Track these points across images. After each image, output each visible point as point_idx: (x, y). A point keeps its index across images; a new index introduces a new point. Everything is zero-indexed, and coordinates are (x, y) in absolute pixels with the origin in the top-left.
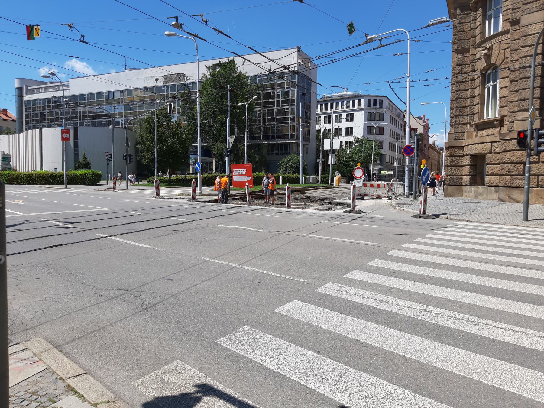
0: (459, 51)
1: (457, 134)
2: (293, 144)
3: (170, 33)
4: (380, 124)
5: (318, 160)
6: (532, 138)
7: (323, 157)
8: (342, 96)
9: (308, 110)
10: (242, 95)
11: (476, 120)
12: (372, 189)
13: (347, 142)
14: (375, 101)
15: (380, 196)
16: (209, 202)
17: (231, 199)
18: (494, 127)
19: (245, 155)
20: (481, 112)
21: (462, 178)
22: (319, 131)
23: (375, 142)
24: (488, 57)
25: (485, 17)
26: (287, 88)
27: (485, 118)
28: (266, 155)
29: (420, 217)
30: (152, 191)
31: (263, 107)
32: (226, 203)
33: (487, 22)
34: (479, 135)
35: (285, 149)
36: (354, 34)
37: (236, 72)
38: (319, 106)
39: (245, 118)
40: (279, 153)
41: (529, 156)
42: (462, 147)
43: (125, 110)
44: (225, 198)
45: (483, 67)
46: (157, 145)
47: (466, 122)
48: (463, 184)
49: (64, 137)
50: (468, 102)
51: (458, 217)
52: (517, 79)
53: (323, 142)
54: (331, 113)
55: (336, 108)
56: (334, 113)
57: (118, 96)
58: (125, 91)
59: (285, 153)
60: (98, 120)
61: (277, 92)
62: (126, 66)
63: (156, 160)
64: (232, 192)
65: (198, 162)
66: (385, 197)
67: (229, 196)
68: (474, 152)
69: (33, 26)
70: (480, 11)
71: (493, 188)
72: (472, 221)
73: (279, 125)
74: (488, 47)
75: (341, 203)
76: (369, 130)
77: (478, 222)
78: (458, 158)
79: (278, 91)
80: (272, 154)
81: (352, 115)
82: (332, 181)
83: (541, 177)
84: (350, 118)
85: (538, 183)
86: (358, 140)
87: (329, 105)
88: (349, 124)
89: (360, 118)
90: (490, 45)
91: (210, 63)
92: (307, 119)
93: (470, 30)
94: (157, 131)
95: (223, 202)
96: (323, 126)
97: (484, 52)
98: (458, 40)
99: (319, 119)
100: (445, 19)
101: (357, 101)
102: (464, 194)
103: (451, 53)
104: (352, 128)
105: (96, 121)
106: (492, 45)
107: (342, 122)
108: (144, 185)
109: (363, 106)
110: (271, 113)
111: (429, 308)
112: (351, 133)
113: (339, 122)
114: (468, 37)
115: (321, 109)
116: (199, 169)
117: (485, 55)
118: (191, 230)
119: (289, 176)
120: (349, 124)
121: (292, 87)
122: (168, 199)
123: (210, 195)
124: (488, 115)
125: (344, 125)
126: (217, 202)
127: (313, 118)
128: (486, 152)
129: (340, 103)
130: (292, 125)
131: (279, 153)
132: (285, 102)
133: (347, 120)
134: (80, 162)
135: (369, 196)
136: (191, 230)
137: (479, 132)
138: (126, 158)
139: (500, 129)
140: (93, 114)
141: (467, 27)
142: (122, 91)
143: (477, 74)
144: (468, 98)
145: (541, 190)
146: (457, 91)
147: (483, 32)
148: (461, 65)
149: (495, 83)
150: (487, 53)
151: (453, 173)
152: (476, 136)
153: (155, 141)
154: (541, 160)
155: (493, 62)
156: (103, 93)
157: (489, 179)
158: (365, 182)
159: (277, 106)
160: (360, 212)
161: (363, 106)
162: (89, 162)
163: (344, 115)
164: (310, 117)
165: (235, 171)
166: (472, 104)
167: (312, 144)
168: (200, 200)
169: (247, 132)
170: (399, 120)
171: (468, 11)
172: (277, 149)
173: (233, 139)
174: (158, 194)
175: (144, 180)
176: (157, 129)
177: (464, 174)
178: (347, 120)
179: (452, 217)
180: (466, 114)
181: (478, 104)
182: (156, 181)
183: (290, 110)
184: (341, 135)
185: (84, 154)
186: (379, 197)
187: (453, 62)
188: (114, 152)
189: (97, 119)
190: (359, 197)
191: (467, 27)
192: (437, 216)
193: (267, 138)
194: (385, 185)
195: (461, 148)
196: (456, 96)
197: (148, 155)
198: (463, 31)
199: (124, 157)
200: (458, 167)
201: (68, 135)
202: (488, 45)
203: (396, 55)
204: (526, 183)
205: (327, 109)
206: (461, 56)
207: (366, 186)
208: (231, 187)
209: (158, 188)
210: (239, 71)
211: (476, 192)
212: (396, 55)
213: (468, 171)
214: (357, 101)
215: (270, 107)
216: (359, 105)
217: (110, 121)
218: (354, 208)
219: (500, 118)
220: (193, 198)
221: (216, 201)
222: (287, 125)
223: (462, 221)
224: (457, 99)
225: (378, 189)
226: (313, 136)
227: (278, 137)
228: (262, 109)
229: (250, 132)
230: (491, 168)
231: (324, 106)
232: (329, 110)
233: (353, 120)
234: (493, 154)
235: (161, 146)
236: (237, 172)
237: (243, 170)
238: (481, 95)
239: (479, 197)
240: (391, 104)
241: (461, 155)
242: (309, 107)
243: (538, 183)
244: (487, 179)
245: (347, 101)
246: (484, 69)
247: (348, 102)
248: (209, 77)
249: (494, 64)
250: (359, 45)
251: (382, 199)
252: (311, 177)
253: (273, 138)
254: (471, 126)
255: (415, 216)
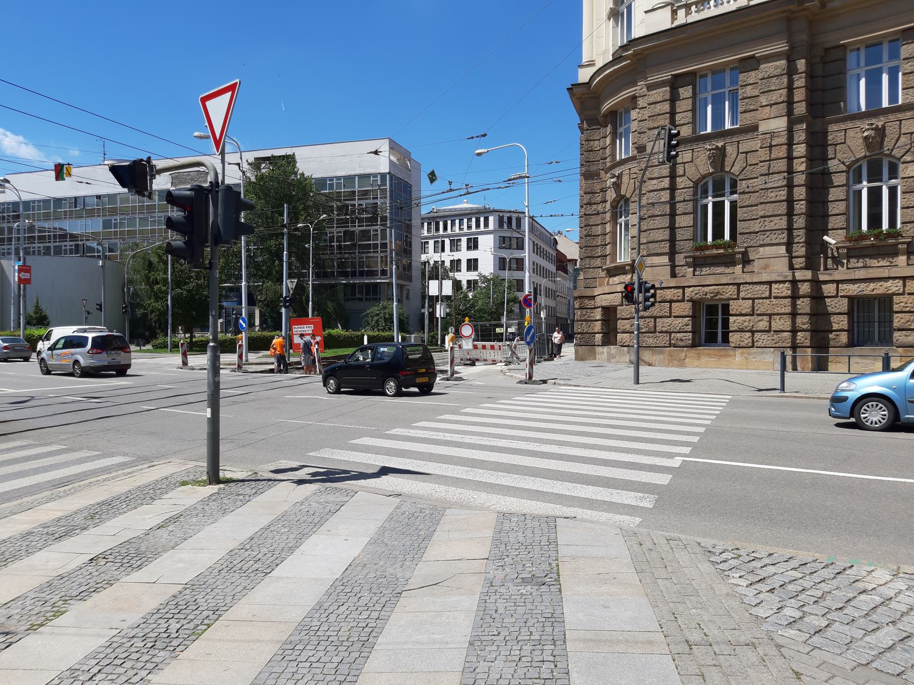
0: (588, 175)
1: (588, 280)
2: (386, 284)
3: (202, 134)
4: (517, 254)
5: (423, 311)
6: (640, 291)
7: (430, 306)
8: (461, 209)
9: (408, 232)
10: (305, 209)
11: (609, 264)
12: (484, 351)
13: (469, 282)
14: (510, 219)
15: (495, 361)
16: (261, 372)
17: (293, 368)
18: (625, 273)
19: (310, 303)
20: (614, 254)
21: (594, 336)
22: (424, 263)
23: (510, 282)
24: (617, 186)
25: (615, 135)
26: (373, 198)
27: (618, 261)
28: (342, 302)
29: (526, 383)
30: (177, 359)
31: (337, 227)
32: (287, 373)
33: (618, 141)
34: (611, 283)
35: (374, 292)
36: (435, 183)
37: (296, 173)
38: (426, 224)
39: (310, 246)
40: (364, 299)
41: (637, 311)
42: (593, 297)
43: (104, 228)
44: (284, 365)
45: (613, 197)
46: (172, 289)
47: (597, 266)
48: (596, 344)
49: (23, 278)
50: (599, 241)
51: (567, 382)
52: (646, 216)
53: (428, 282)
54: (443, 236)
55: (452, 229)
56: (448, 236)
57: (93, 204)
58: (105, 196)
59: (374, 299)
60: (55, 244)
61: (360, 205)
62: (105, 154)
63: (170, 313)
64: (292, 360)
65: (243, 316)
66: (501, 362)
67: (290, 364)
68: (604, 304)
69: (63, 165)
70: (609, 129)
71: (626, 349)
72: (579, 386)
73: (363, 255)
74: (617, 175)
75: (443, 371)
76: (502, 264)
77: (585, 386)
78: (589, 310)
79: (361, 202)
80: (352, 299)
81: (476, 241)
82: (443, 341)
83: (673, 335)
84: (473, 244)
85: (670, 342)
86: (485, 279)
87: (441, 224)
88: (472, 254)
89: (487, 242)
90: (619, 172)
91: (250, 157)
92: (406, 250)
93: (599, 150)
94: (173, 268)
95: (280, 371)
96: (431, 256)
97: (613, 180)
98: (586, 162)
99: (426, 246)
100: (524, 175)
101: (482, 219)
102: (598, 356)
103: (578, 176)
104: (476, 260)
105: (52, 245)
106: (622, 172)
107: (461, 251)
108: (148, 351)
109: (491, 226)
110: (349, 235)
111: (463, 436)
112: (476, 268)
113: (457, 250)
114: (597, 159)
115: (429, 230)
116: (244, 326)
117: (614, 183)
118: (253, 401)
119: (378, 335)
120: (472, 254)
121: (381, 198)
122: (201, 369)
123: (261, 364)
124: (620, 259)
125: (464, 255)
126: (274, 373)
127: (416, 246)
128: (617, 304)
129: (457, 221)
130: (382, 254)
131: (364, 299)
132: (373, 220)
133: (469, 248)
134: (30, 315)
135: (482, 361)
136: (253, 401)
137: (611, 279)
138: (126, 311)
139: (632, 276)
140: (47, 234)
141: (596, 145)
142: (99, 197)
143: (608, 205)
144: (599, 236)
145: (673, 350)
146: (585, 226)
147: (613, 155)
148: (589, 193)
149: (627, 219)
150: (616, 182)
151: (584, 330)
152: (608, 284)
153: (168, 283)
154: (673, 314)
155: (623, 193)
156: (65, 199)
157: (621, 337)
158: (476, 343)
159: (359, 226)
160: (461, 379)
161: (491, 226)
162: (45, 315)
163: (464, 240)
164: (411, 243)
165: (297, 329)
166: (603, 243)
167: (416, 284)
168: (249, 370)
169: (313, 268)
170: (547, 248)
171: (597, 125)
172: (361, 292)
173: (295, 284)
174: (185, 363)
175: (148, 342)
176: (173, 265)
177: (596, 331)
178: (469, 248)
179: (560, 382)
180: (596, 255)
181: (609, 243)
182: (182, 344)
183: (379, 232)
184: (460, 271)
185: (37, 302)
186: (494, 362)
187: (581, 189)
188: (104, 302)
189: (54, 242)
190: (469, 362)
191: (596, 145)
192: (545, 382)
193: (345, 275)
194: (500, 346)
195: (591, 298)
196: (585, 233)
197: (158, 305)
198: (592, 151)
199: (123, 308)
200: (589, 323)
201: (28, 274)
202: (617, 172)
203: (500, 188)
204: (635, 341)
205: (437, 230)
206: (590, 182)
207: (477, 348)
208: (291, 351)
209: (185, 355)
210: (300, 172)
211: (609, 354)
212: (500, 188)
213: (600, 328)
214: (482, 219)
215: (348, 227)
216: (486, 225)
217: (77, 246)
218: (452, 375)
219: (631, 262)
220: (240, 367)
221: (272, 371)
222: (375, 255)
223: (570, 386)
224: (587, 236)
225: (492, 352)
226: (416, 273)
227: (362, 274)
228: (336, 231)
229: (316, 265)
230: (622, 324)
231: (433, 227)
232: (441, 232)
233: (478, 248)
234: (624, 306)
235: (178, 290)
236: (299, 330)
237: (309, 327)
238: (613, 233)
239: (612, 360)
240: (534, 223)
241: (593, 306)
242: (409, 228)
243: (670, 342)
244: (619, 336)
245: (468, 219)
246: (614, 200)
247: (469, 220)
248: (253, 179)
249: (625, 196)
250: (443, 192)
251: (498, 364)
252: (413, 336)
253: (354, 274)
254: (603, 270)
255: (520, 382)
